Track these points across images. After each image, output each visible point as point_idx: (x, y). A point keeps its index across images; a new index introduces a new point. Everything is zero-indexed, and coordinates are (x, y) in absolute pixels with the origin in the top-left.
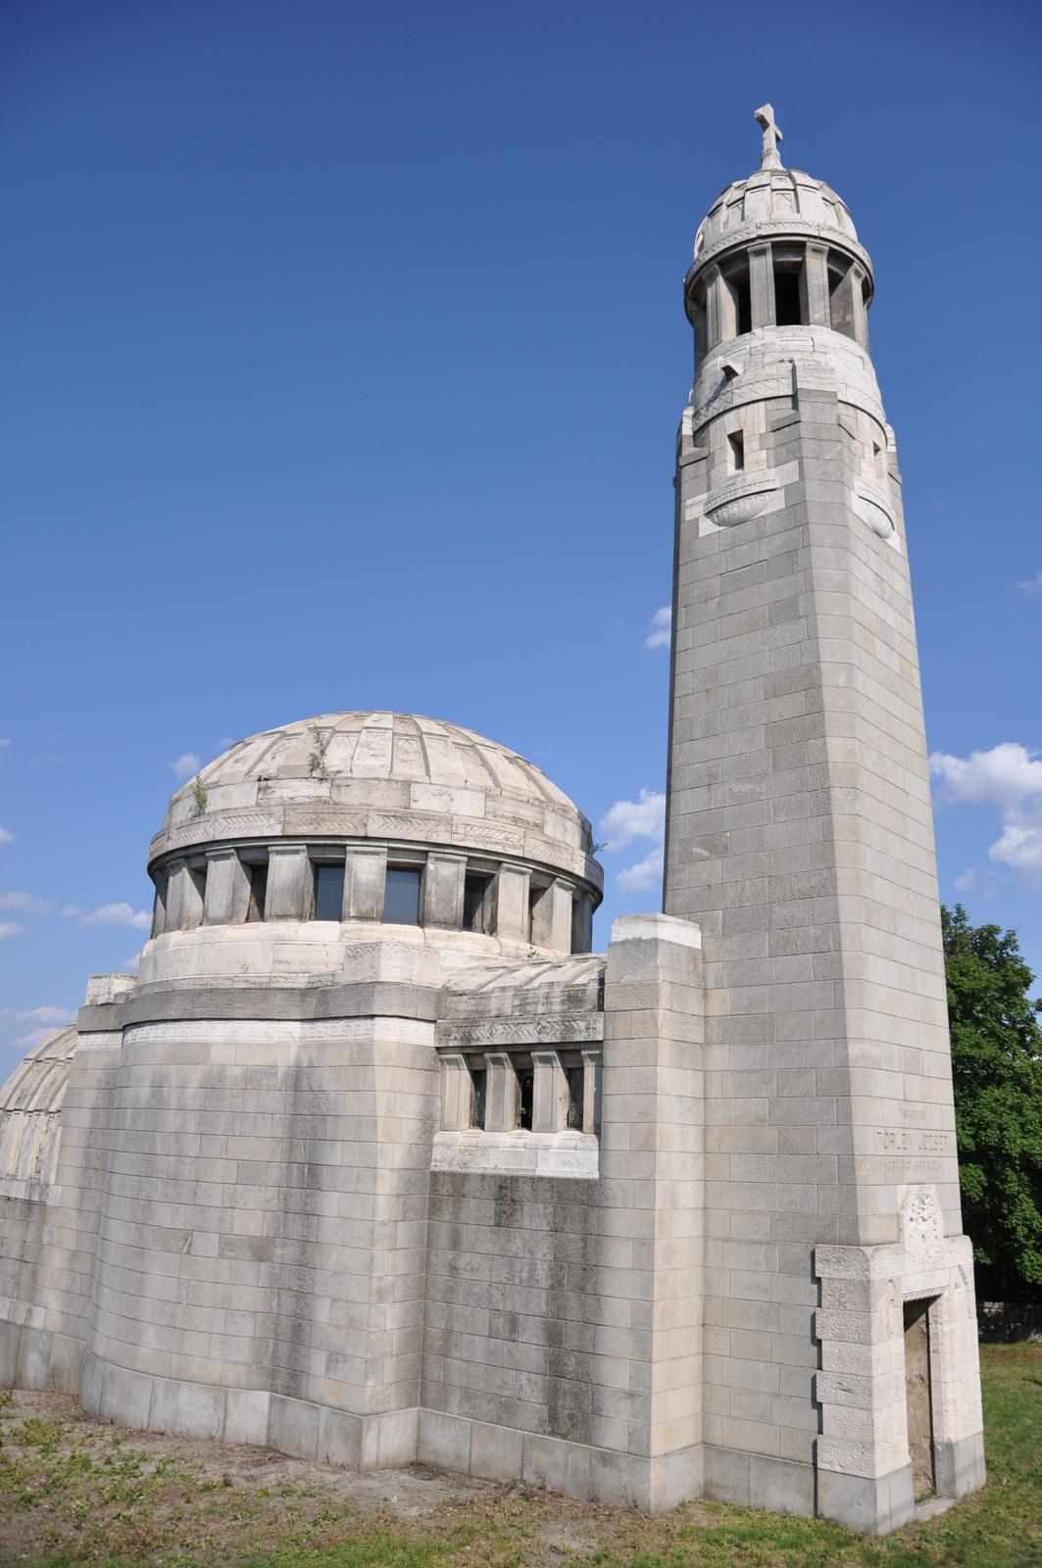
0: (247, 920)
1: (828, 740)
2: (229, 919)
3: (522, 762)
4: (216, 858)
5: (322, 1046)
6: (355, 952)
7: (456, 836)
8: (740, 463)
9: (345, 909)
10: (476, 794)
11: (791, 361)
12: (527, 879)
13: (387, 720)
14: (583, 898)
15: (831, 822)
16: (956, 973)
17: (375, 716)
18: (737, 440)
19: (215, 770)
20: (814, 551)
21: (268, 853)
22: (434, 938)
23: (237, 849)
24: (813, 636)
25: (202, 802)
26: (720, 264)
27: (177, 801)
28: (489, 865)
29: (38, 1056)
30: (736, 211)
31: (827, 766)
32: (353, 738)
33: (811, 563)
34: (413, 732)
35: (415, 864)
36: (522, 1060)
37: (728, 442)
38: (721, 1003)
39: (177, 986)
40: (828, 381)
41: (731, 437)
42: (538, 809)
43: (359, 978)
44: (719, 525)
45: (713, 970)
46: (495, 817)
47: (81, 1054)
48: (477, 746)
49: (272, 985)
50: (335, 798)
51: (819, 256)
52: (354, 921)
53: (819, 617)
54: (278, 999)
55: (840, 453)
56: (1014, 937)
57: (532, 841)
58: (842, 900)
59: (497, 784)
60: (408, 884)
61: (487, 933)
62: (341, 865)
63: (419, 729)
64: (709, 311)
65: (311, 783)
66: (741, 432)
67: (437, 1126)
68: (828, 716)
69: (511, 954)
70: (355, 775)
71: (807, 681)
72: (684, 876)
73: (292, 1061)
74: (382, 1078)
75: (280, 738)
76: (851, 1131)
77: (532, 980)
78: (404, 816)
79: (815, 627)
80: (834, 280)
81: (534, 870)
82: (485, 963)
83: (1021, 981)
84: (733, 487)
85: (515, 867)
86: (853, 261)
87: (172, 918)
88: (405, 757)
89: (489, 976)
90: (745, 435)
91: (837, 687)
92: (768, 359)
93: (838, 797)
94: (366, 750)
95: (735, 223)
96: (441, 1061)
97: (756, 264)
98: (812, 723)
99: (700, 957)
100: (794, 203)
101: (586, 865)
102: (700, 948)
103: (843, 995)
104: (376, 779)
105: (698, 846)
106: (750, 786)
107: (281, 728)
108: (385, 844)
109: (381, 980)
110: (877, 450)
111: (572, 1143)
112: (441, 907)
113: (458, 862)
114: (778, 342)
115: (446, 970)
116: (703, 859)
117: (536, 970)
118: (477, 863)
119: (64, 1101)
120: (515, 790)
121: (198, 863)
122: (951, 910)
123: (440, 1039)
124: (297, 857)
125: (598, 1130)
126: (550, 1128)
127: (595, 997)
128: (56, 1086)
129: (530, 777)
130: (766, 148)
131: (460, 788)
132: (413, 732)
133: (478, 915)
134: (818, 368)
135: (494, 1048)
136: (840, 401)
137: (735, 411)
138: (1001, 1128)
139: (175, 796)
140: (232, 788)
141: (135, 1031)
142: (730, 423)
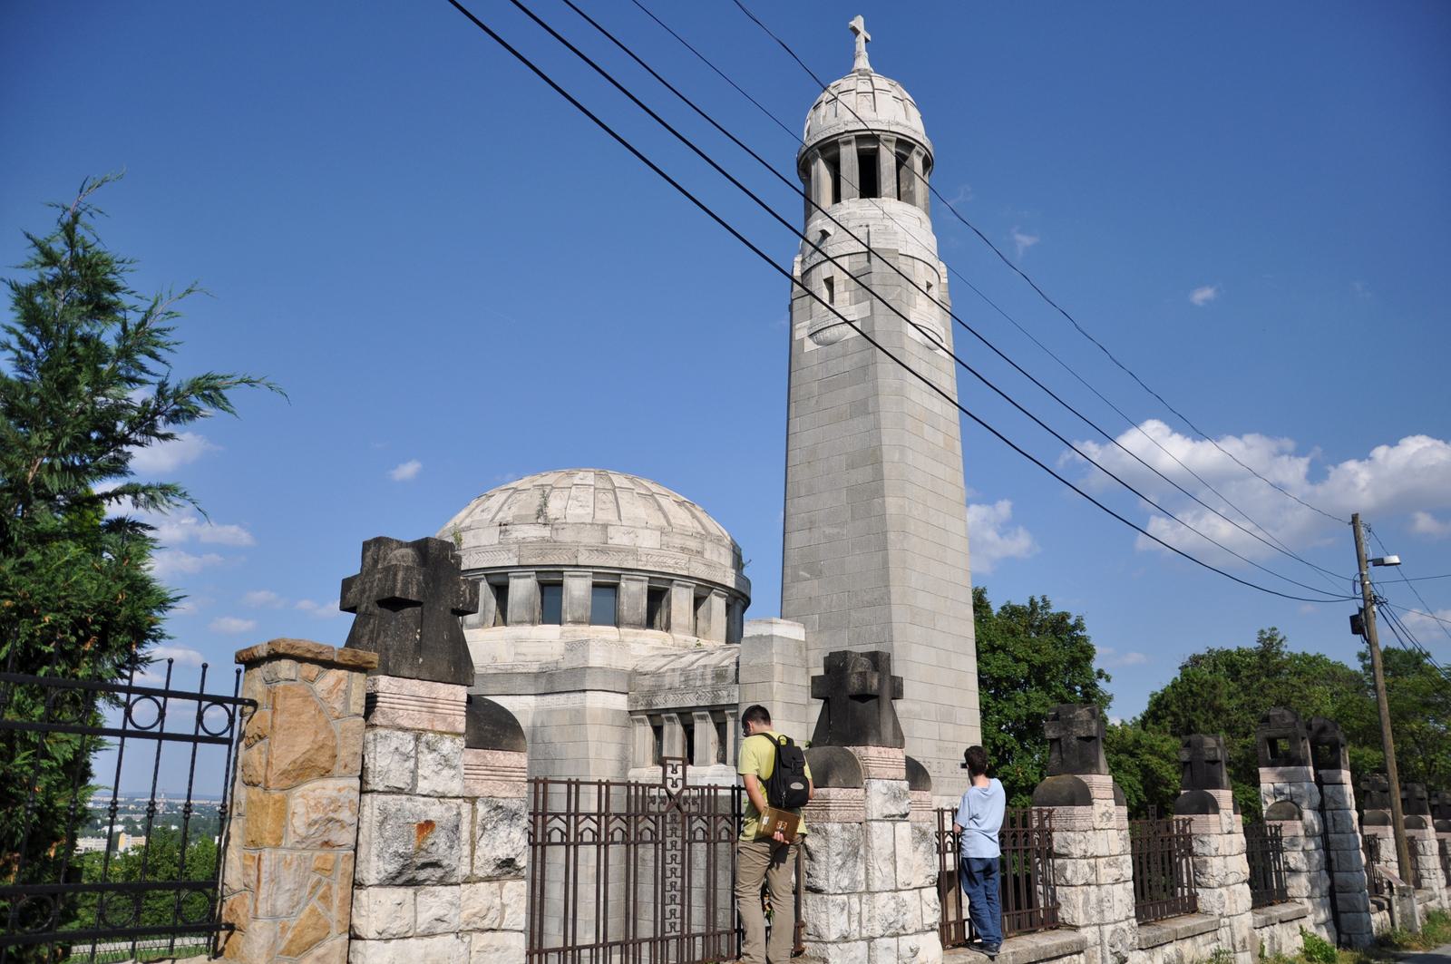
0: (494, 625)
1: (886, 499)
5: (550, 712)
6: (572, 647)
11: (867, 226)
12: (692, 591)
13: (587, 477)
14: (735, 603)
15: (887, 555)
18: (829, 283)
19: (467, 517)
21: (508, 578)
22: (626, 635)
23: (486, 575)
24: (877, 427)
30: (831, 107)
32: (566, 493)
34: (609, 487)
36: (686, 717)
41: (826, 280)
43: (574, 665)
50: (555, 538)
54: (519, 681)
55: (900, 295)
58: (894, 608)
59: (670, 524)
60: (607, 597)
62: (560, 584)
63: (613, 484)
64: (813, 183)
65: (537, 527)
67: (631, 765)
70: (568, 521)
71: (872, 458)
74: (593, 732)
75: (514, 493)
77: (693, 663)
80: (901, 161)
82: (663, 652)
83: (1063, 656)
88: (603, 506)
89: (665, 661)
95: (831, 120)
102: (803, 639)
106: (836, 530)
107: (513, 485)
111: (719, 773)
113: (642, 581)
114: (858, 211)
115: (636, 657)
117: (696, 657)
122: (1038, 599)
124: (529, 580)
125: (736, 764)
126: (705, 763)
127: (734, 674)
129: (694, 516)
130: (857, 49)
131: (642, 528)
132: (609, 487)
133: (657, 617)
134: (886, 231)
135: (667, 710)
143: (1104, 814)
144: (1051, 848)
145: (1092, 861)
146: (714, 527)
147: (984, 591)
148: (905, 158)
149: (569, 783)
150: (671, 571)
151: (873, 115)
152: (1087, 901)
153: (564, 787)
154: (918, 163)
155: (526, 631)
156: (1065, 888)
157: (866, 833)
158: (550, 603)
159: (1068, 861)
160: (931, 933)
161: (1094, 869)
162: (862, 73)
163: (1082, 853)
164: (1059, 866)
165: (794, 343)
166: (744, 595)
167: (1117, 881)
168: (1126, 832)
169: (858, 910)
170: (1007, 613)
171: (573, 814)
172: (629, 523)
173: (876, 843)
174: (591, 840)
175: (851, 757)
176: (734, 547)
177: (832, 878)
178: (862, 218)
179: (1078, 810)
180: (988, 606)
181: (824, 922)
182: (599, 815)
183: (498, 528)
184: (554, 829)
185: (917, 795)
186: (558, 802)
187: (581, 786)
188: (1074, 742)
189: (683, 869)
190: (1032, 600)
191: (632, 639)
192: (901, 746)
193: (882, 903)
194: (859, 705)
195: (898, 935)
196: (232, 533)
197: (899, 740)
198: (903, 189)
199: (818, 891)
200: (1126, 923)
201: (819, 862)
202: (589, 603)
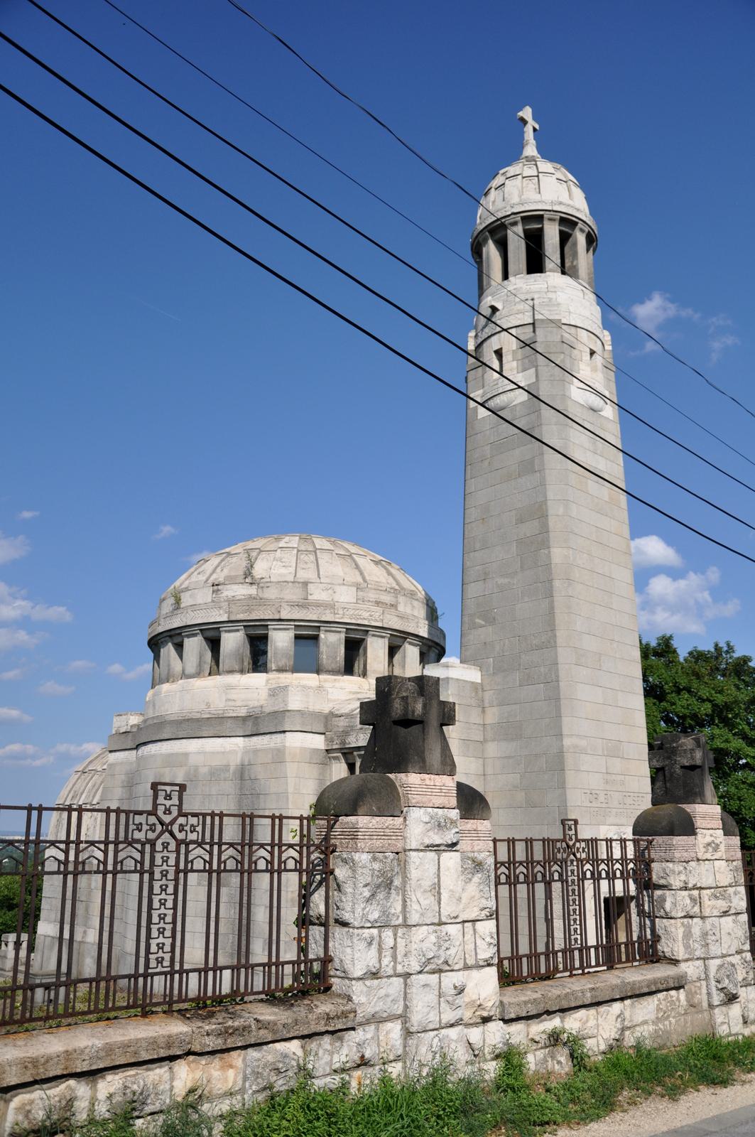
0: (210, 674)
1: (552, 550)
2: (198, 674)
3: (384, 563)
4: (188, 636)
5: (256, 751)
6: (274, 692)
9: (269, 665)
11: (533, 299)
13: (294, 541)
14: (429, 651)
15: (553, 601)
17: (287, 539)
18: (499, 353)
19: (186, 579)
21: (220, 632)
23: (201, 630)
24: (543, 484)
25: (178, 601)
26: (489, 232)
27: (164, 600)
28: (361, 633)
29: (85, 768)
32: (272, 555)
34: (311, 548)
38: (492, 716)
39: (168, 718)
43: (276, 709)
45: (488, 696)
47: (111, 766)
49: (225, 715)
50: (261, 595)
52: (274, 672)
53: (547, 471)
54: (229, 724)
57: (388, 616)
58: (559, 650)
60: (307, 646)
63: (315, 546)
64: (484, 264)
65: (245, 586)
66: (501, 349)
68: (551, 535)
71: (539, 512)
73: (238, 761)
74: (291, 769)
75: (226, 557)
76: (565, 792)
78: (303, 605)
80: (565, 238)
84: (496, 387)
87: (163, 676)
90: (504, 351)
91: (558, 515)
94: (279, 563)
95: (500, 204)
96: (329, 758)
98: (542, 540)
99: (479, 688)
100: (537, 186)
101: (429, 629)
102: (480, 681)
103: (560, 710)
104: (285, 582)
106: (506, 580)
108: (292, 623)
109: (289, 709)
110: (592, 353)
112: (330, 661)
113: (340, 632)
114: (524, 286)
115: (334, 701)
116: (482, 626)
118: (356, 632)
119: (101, 796)
121: (177, 640)
122: (723, 645)
123: (328, 744)
128: (96, 788)
129: (389, 573)
130: (526, 138)
131: (339, 585)
133: (356, 665)
138: (740, 799)
139: (163, 597)
140: (196, 591)
141: (143, 748)
142: (494, 343)
143: (709, 844)
144: (650, 879)
145: (695, 893)
146: (408, 582)
147: (671, 638)
149: (273, 817)
151: (537, 197)
152: (688, 935)
153: (269, 821)
154: (581, 239)
155: (236, 679)
156: (665, 920)
157: (403, 866)
158: (258, 655)
159: (668, 893)
160: (488, 969)
161: (697, 901)
162: (531, 160)
163: (682, 885)
164: (659, 897)
165: (469, 412)
166: (437, 644)
167: (725, 913)
168: (739, 864)
169: (392, 944)
170: (693, 657)
171: (277, 844)
172: (328, 580)
173: (414, 873)
174: (264, 868)
175: (392, 785)
176: (427, 601)
177: (359, 911)
178: (528, 292)
179: (678, 840)
180: (675, 651)
181: (349, 957)
182: (272, 845)
183: (211, 588)
184: (289, 858)
185: (471, 824)
186: (263, 833)
187: (284, 821)
188: (678, 771)
189: (175, 901)
190: (716, 645)
192: (452, 772)
193: (421, 937)
194: (402, 731)
195: (440, 971)
196: (58, 613)
197: (448, 767)
198: (567, 264)
199: (345, 924)
200: (738, 957)
201: (345, 894)
202: (292, 653)
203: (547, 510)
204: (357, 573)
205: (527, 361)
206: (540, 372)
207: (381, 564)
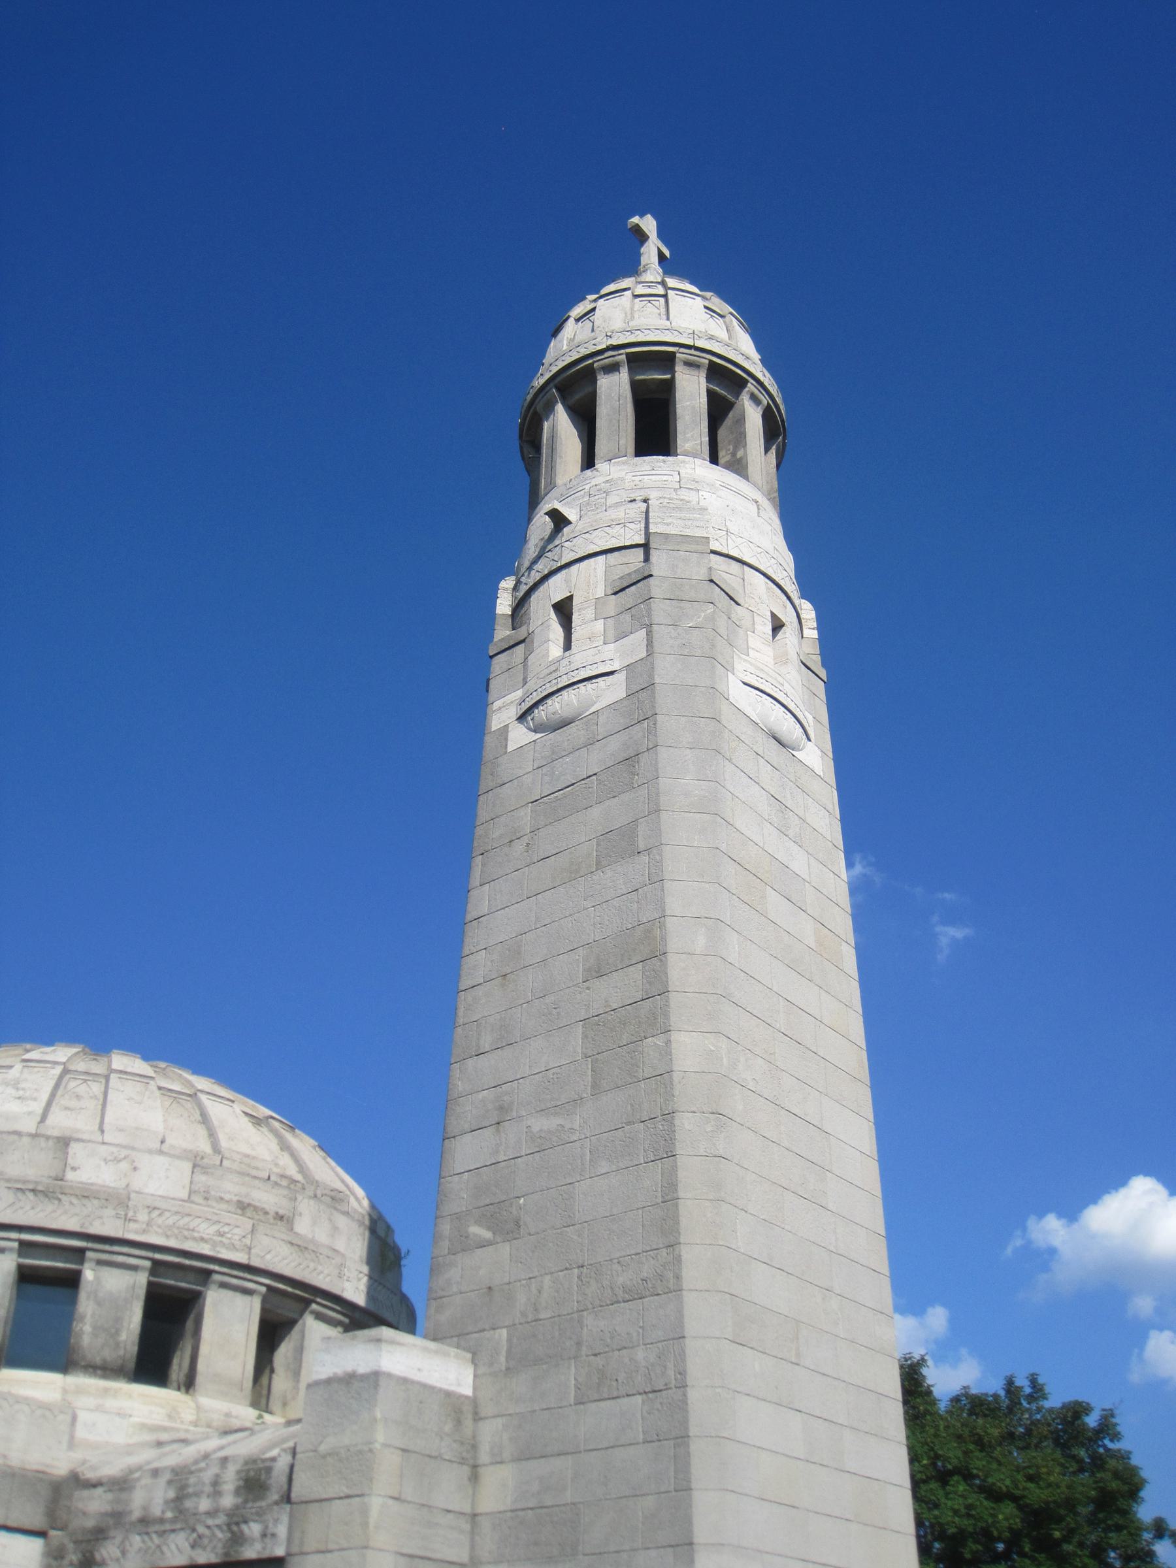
1: (675, 1036)
3: (276, 1124)
7: (132, 1225)
8: (568, 646)
10: (177, 1162)
11: (645, 501)
12: (256, 1303)
15: (674, 1168)
16: (1020, 1477)
20: (663, 753)
22: (79, 1391)
24: (657, 880)
26: (558, 389)
31: (671, 1077)
33: (657, 770)
35: (40, 1259)
37: (552, 612)
40: (695, 523)
42: (285, 1192)
44: (535, 731)
46: (206, 1199)
48: (199, 1094)
51: (696, 373)
53: (667, 850)
55: (712, 618)
56: (1114, 1420)
57: (266, 1241)
58: (689, 1298)
59: (216, 1148)
61: (183, 1389)
64: (544, 451)
66: (570, 598)
68: (674, 999)
69: (215, 1424)
71: (646, 948)
72: (454, 1273)
79: (660, 865)
81: (269, 1287)
84: (554, 675)
85: (235, 1281)
86: (747, 382)
92: (612, 499)
93: (687, 1127)
97: (605, 383)
98: (650, 1012)
99: (467, 1409)
102: (468, 1391)
103: (687, 1465)
104: (16, 1133)
105: (478, 1223)
106: (559, 1121)
113: (134, 1268)
116: (483, 1244)
120: (246, 1160)
122: (1022, 1382)
127: (284, 1479)
129: (285, 1146)
130: (643, 263)
131: (150, 1152)
133: (175, 1361)
136: (713, 552)
137: (564, 572)
142: (556, 589)
146: (327, 1171)
148: (729, 406)
150: (206, 1250)
154: (753, 418)
172: (120, 1139)
178: (636, 488)
191: (90, 1402)
203: (664, 939)
204: (202, 1132)
205: (627, 617)
206: (656, 636)
207: (268, 1125)
